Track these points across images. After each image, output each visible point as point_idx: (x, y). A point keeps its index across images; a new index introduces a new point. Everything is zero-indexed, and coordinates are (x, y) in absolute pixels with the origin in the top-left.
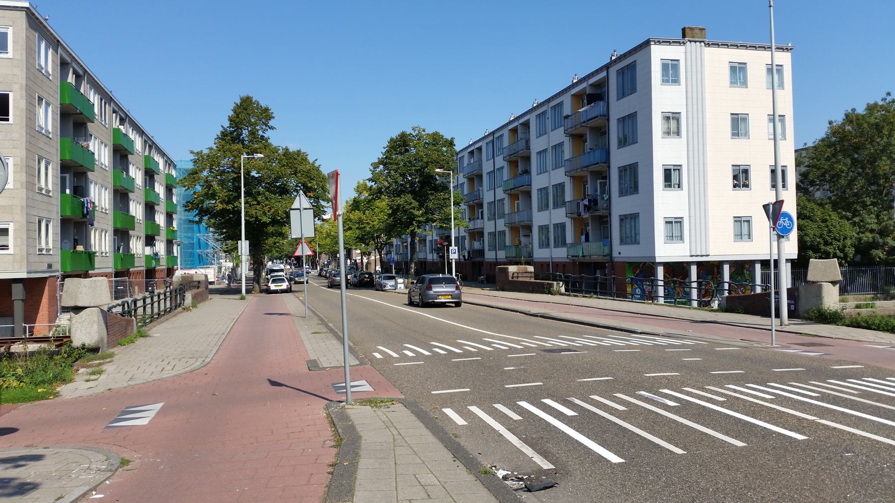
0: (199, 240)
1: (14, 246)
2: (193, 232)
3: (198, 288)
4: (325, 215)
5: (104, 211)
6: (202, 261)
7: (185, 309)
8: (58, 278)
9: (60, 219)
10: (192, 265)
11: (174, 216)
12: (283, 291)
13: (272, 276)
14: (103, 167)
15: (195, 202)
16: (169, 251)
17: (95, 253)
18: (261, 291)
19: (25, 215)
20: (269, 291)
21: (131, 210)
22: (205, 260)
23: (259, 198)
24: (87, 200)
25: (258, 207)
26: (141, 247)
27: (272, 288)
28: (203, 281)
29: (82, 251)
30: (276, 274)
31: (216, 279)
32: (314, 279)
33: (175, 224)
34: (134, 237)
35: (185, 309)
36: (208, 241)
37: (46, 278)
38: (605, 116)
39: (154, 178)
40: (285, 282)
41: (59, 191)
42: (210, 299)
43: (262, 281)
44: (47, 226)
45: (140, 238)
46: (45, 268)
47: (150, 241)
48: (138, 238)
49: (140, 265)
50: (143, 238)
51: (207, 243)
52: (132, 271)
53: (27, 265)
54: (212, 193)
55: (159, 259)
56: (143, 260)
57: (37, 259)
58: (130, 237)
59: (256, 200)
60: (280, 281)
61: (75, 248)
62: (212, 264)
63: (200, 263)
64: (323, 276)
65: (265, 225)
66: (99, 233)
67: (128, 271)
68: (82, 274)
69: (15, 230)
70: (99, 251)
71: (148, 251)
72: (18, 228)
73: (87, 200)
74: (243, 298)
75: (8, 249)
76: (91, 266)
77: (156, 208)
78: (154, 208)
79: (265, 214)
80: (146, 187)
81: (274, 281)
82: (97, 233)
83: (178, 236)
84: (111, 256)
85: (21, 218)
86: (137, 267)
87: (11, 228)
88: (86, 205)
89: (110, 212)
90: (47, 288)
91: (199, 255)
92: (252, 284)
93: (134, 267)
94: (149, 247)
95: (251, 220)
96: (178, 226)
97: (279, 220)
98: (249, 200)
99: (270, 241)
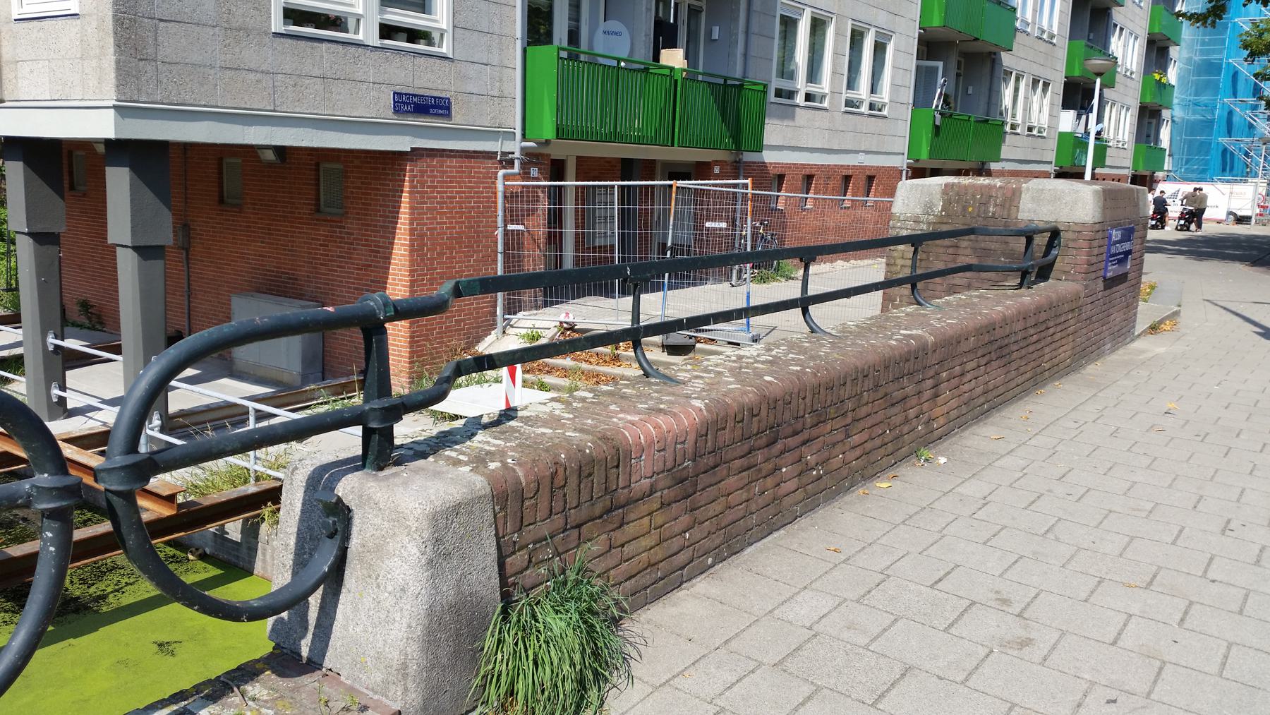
0: (1230, 113)
2: (1216, 92)
3: (1044, 273)
9: (917, 36)
11: (1174, 52)
22: (1238, 166)
26: (1046, 109)
28: (1079, 229)
31: (1258, 211)
33: (1172, 75)
34: (1113, 104)
37: (394, 159)
38: (914, 287)
41: (1068, 37)
45: (1046, 85)
50: (1057, 88)
56: (1053, 144)
61: (656, 58)
62: (1256, 176)
63: (1224, 170)
66: (1117, 111)
68: (716, 162)
70: (1024, 122)
71: (1067, 121)
82: (1114, 110)
84: (1130, 148)
90: (405, 198)
91: (1225, 151)
93: (998, 160)
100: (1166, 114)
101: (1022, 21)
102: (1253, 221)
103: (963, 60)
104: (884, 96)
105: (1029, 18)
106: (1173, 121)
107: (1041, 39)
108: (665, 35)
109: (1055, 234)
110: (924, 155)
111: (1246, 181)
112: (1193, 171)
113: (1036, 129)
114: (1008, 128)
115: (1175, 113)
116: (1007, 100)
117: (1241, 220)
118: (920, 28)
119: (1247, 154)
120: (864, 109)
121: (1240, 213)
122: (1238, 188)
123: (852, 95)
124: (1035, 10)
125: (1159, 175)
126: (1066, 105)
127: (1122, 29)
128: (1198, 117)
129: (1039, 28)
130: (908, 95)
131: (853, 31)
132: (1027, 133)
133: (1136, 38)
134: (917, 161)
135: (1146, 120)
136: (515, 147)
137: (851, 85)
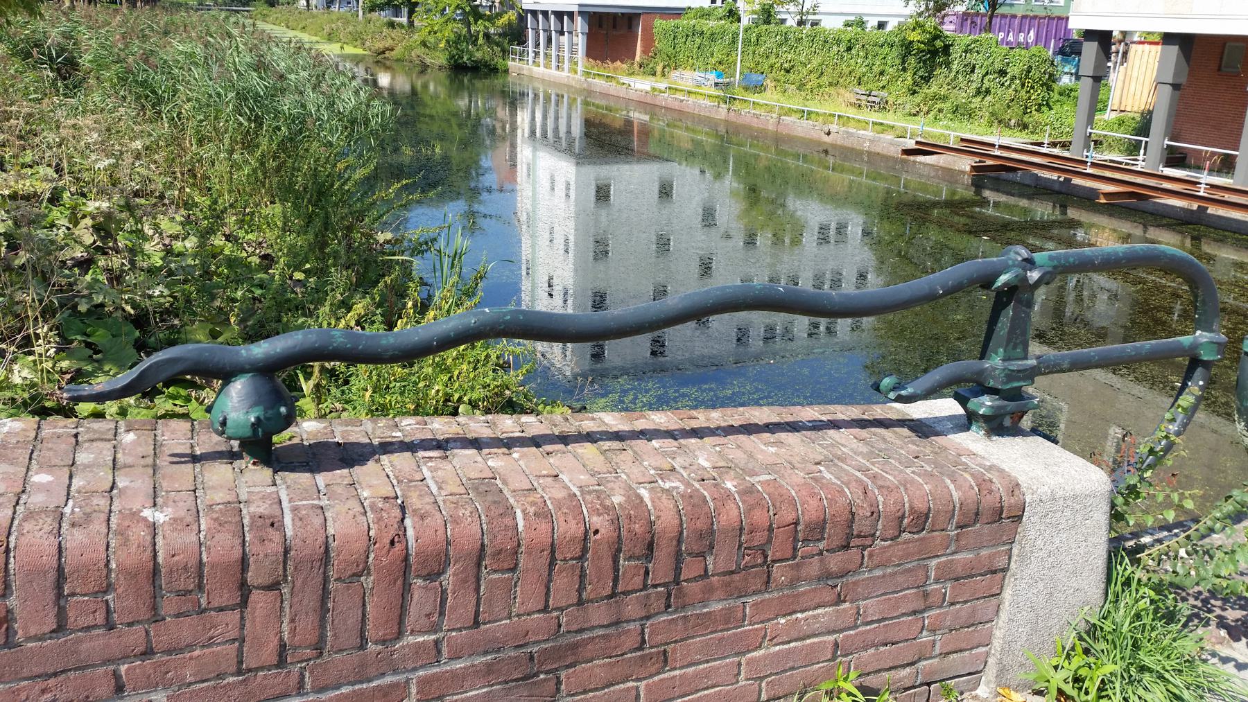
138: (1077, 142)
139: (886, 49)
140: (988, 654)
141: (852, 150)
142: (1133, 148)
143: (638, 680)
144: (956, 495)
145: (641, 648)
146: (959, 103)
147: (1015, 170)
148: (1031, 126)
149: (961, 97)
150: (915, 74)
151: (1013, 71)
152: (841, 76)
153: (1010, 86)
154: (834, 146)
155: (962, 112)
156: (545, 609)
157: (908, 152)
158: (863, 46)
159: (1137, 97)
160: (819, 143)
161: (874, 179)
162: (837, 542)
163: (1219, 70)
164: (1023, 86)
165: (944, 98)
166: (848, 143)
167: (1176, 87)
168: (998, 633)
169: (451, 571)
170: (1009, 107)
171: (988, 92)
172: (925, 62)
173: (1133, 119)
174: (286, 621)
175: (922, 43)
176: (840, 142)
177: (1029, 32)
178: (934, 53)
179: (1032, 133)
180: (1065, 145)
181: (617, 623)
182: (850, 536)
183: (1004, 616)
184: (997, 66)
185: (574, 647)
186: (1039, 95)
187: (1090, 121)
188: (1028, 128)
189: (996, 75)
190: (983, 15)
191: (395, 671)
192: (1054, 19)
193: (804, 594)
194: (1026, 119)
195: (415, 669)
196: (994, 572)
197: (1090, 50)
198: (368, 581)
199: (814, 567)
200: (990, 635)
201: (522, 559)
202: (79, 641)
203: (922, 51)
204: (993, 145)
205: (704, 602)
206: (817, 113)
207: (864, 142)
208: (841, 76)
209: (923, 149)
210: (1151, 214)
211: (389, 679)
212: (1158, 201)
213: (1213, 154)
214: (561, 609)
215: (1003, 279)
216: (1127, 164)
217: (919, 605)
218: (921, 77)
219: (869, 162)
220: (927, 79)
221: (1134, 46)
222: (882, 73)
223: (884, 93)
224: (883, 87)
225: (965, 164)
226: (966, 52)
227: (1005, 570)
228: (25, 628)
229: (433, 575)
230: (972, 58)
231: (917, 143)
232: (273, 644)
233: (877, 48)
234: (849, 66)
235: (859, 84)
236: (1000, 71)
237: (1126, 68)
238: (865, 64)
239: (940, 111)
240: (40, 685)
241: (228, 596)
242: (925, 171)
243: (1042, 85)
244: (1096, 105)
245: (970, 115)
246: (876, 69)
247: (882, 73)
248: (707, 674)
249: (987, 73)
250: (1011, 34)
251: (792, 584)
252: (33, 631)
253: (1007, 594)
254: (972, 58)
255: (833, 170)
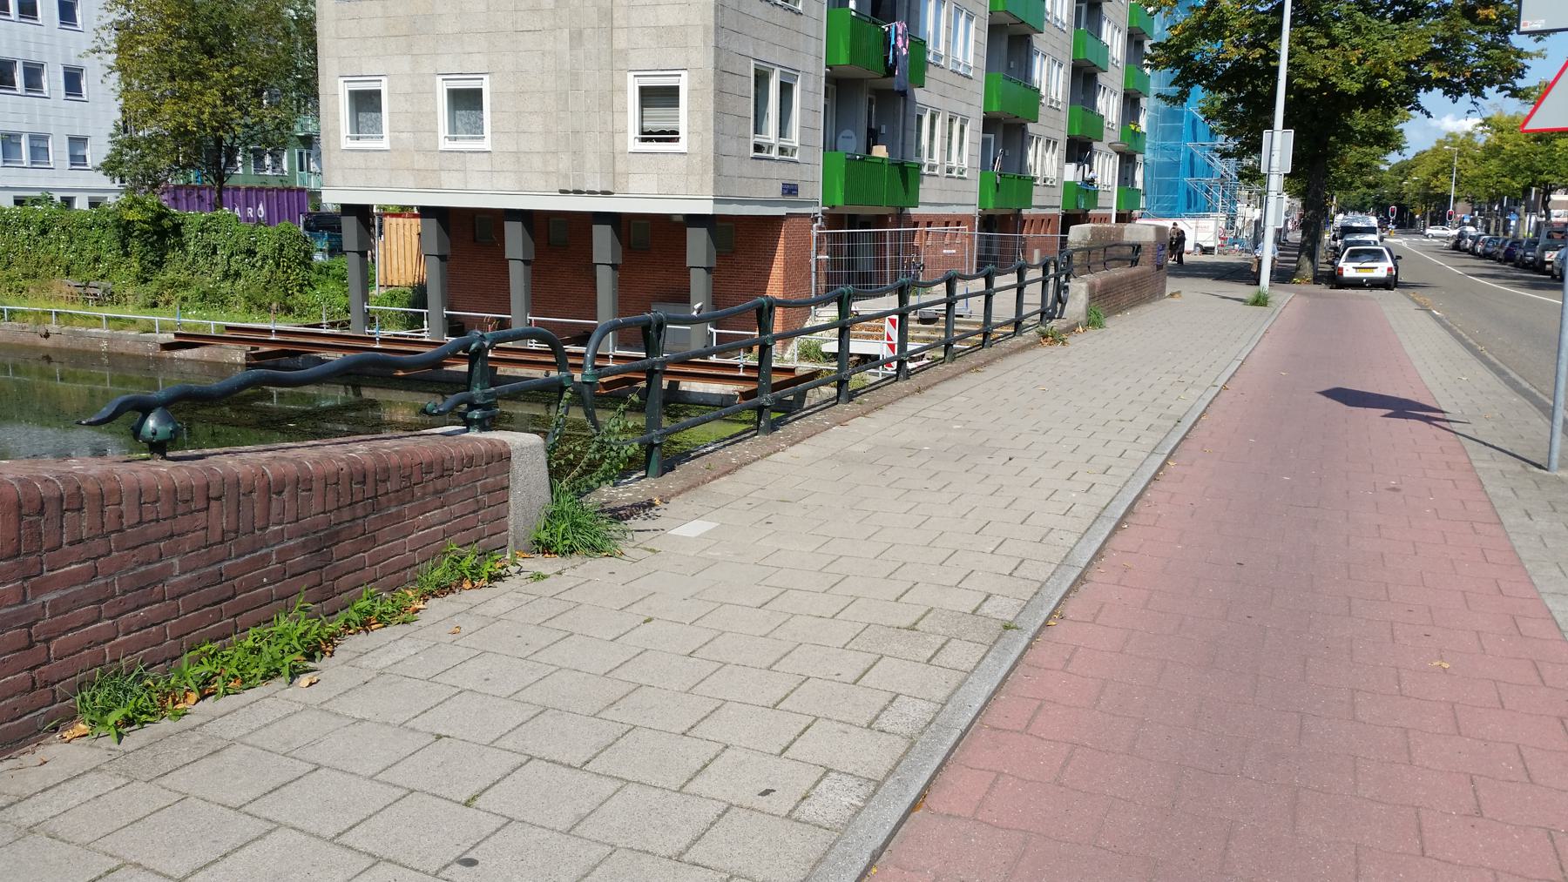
0: (1192, 155)
1: (689, 133)
3: (1135, 262)
4: (1522, 77)
5: (1053, 105)
6: (1195, 204)
7: (1045, 337)
8: (816, 220)
9: (824, 75)
10: (1170, 210)
11: (1143, 102)
12: (1376, 284)
13: (1346, 242)
14: (1059, 25)
15: (1172, 43)
16: (1125, 177)
17: (1034, 179)
18: (1318, 279)
19: (712, 49)
20: (1335, 280)
21: (1036, 76)
22: (1201, 203)
23: (1337, 30)
24: (896, 28)
25: (1329, 52)
26: (1055, 164)
27: (1346, 274)
28: (1149, 244)
29: (883, 159)
30: (1358, 237)
32: (1445, 255)
33: (1143, 123)
34: (1100, 154)
35: (1045, 337)
36: (1213, 161)
37: (777, 220)
39: (1101, 9)
40: (1385, 260)
42: (1172, 295)
43: (1321, 252)
44: (962, 129)
45: (1055, 143)
46: (775, 192)
47: (1079, 150)
48: (1051, 143)
49: (1046, 202)
50: (1062, 145)
51: (1209, 165)
52: (1029, 216)
53: (716, 182)
54: (1215, 20)
55: (1096, 192)
56: (1060, 192)
57: (750, 168)
58: (1027, 139)
59: (1327, 35)
60: (1371, 258)
61: (869, 151)
62: (1216, 210)
63: (1189, 207)
64: (1466, 250)
65: (1345, 102)
67: (1018, 215)
68: (890, 215)
69: (691, 91)
71: (1071, 172)
72: (697, 86)
73: (896, 28)
74: (1260, 301)
75: (677, 140)
76: (906, 191)
77: (1102, 78)
78: (1096, 79)
79: (1348, 69)
80: (1077, 25)
81: (1354, 256)
83: (1147, 145)
85: (703, 58)
86: (1100, 208)
87: (683, 83)
88: (893, 42)
89: (981, 76)
90: (781, 242)
92: (755, 375)
93: (1030, 207)
94: (1074, 165)
95: (1309, 86)
96: (1149, 125)
97: (1386, 88)
98: (1310, 34)
99: (1353, 154)
100: (1139, 158)
101: (965, 65)
102: (1216, 251)
103: (874, 97)
104: (770, 136)
105: (942, 51)
106: (1145, 164)
107: (956, 72)
108: (873, 138)
109: (1139, 246)
110: (839, 201)
111: (1208, 217)
112: (1163, 209)
113: (956, 171)
114: (925, 170)
115: (1146, 156)
116: (1030, 159)
117: (1206, 251)
118: (827, 67)
119: (1207, 191)
120: (774, 154)
121: (1205, 245)
122: (1203, 222)
123: (760, 139)
124: (947, 42)
125: (1136, 213)
126: (1069, 160)
127: (1105, 89)
128: (1166, 160)
129: (953, 61)
130: (977, 162)
131: (756, 70)
132: (946, 174)
133: (1115, 95)
134: (833, 207)
135: (1124, 165)
136: (817, 210)
137: (949, 158)
138: (355, 317)
139: (96, 232)
140: (507, 536)
141: (85, 352)
142: (415, 321)
143: (365, 552)
144: (482, 448)
145: (364, 534)
146: (206, 289)
147: (297, 354)
148: (296, 310)
149: (208, 282)
150: (142, 259)
151: (263, 249)
152: (38, 265)
153: (262, 267)
154: (59, 350)
155: (219, 301)
156: (324, 513)
157: (168, 347)
158: (64, 228)
159: (402, 271)
160: (35, 348)
161: (123, 385)
162: (438, 474)
163: (475, 241)
164: (278, 265)
165: (186, 285)
166: (77, 345)
167: (442, 258)
168: (510, 523)
169: (286, 490)
170: (267, 289)
171: (237, 275)
172: (152, 244)
173: (404, 293)
174: (224, 517)
175: (144, 222)
176: (65, 343)
177: (258, 207)
178: (162, 234)
179: (299, 315)
180: (344, 325)
181: (353, 520)
182: (444, 470)
183: (511, 512)
184: (243, 245)
185: (337, 533)
186: (298, 274)
187: (365, 297)
188: (293, 312)
189: (244, 256)
190: (211, 189)
191: (267, 547)
192: (283, 191)
193: (428, 502)
194: (289, 301)
195: (274, 545)
196: (503, 489)
197: (350, 225)
198: (254, 495)
199: (431, 488)
200: (507, 525)
201: (314, 484)
202: (146, 529)
203: (147, 232)
204: (269, 331)
205: (388, 507)
206: (23, 312)
207: (100, 342)
208: (38, 265)
209: (186, 341)
210: (447, 383)
211: (264, 551)
212: (450, 368)
213: (492, 318)
214: (330, 512)
215: (474, 346)
216: (410, 337)
217: (475, 507)
218: (152, 262)
219: (112, 365)
220: (159, 265)
221: (387, 220)
222: (97, 260)
223: (105, 283)
224: (103, 277)
225: (237, 355)
226: (202, 231)
227: (508, 487)
228: (128, 521)
229: (279, 493)
230: (212, 238)
231: (177, 335)
232: (219, 531)
233: (84, 231)
234: (48, 253)
235: (68, 274)
236: (248, 250)
237: (384, 242)
238: (70, 250)
239: (184, 299)
240: (132, 553)
241: (202, 505)
242: (188, 368)
243: (299, 264)
244: (367, 281)
245: (224, 302)
246: (88, 255)
247: (97, 260)
248: (391, 548)
249: (232, 254)
250: (237, 209)
251: (423, 497)
252: (131, 523)
253: (511, 500)
254: (212, 238)
255: (62, 379)
